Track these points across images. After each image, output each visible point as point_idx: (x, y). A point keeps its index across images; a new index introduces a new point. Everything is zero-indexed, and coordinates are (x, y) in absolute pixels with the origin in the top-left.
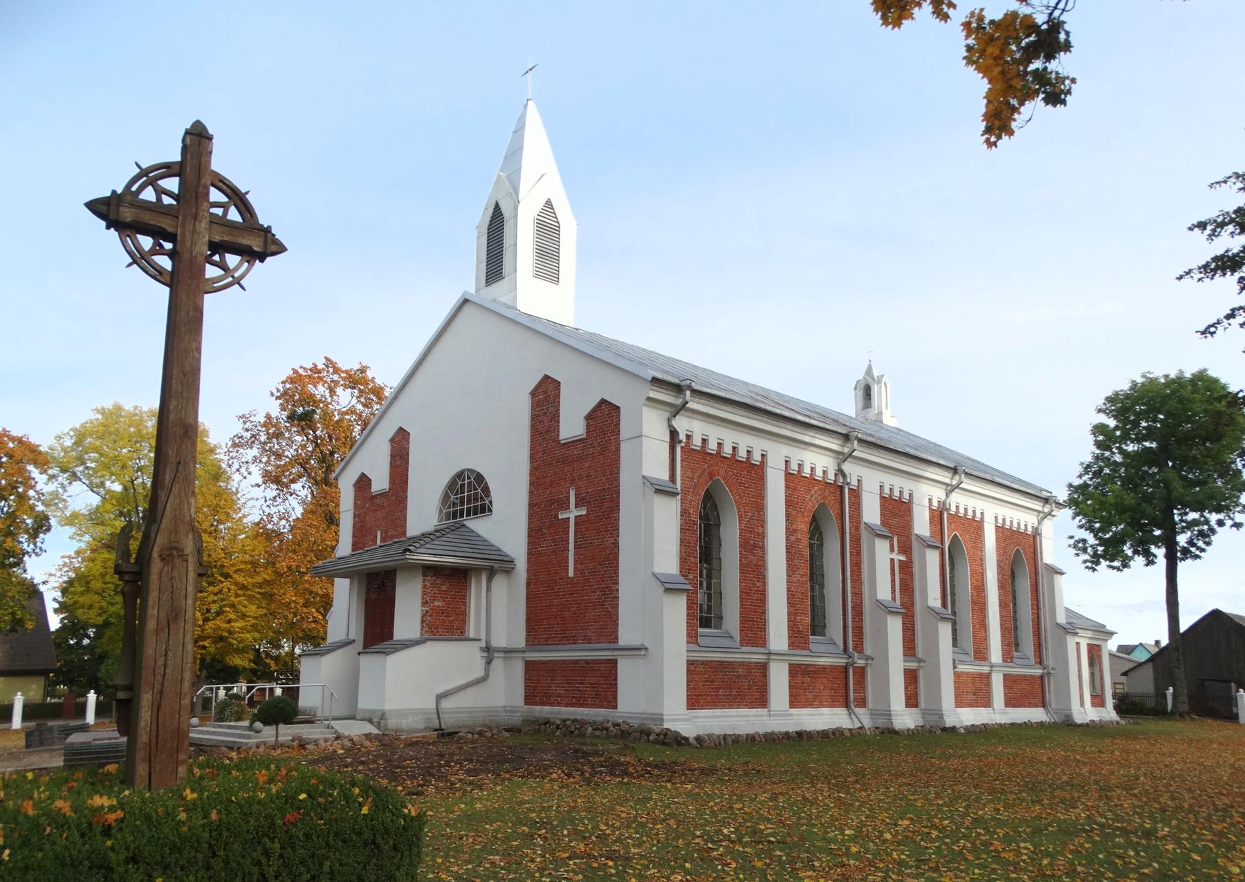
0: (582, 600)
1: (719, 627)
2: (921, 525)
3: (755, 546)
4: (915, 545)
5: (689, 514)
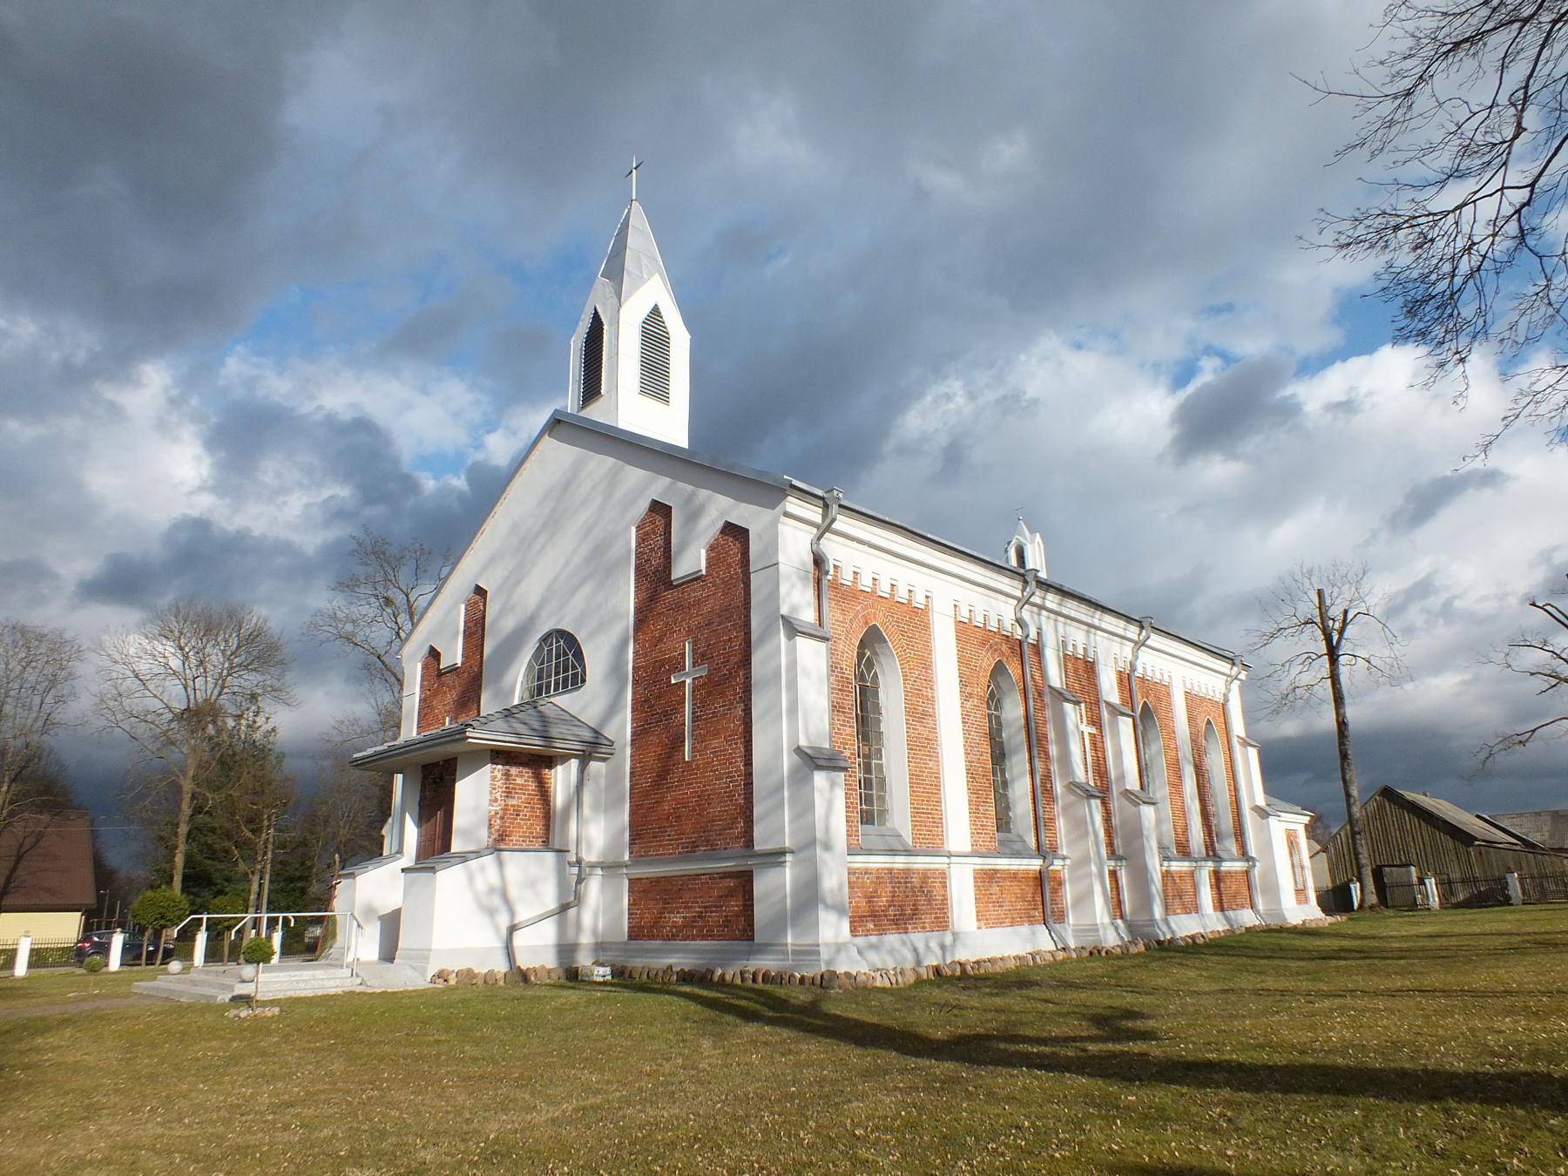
0: (703, 791)
1: (882, 823)
2: (1110, 689)
3: (925, 714)
4: (1105, 715)
5: (842, 669)
